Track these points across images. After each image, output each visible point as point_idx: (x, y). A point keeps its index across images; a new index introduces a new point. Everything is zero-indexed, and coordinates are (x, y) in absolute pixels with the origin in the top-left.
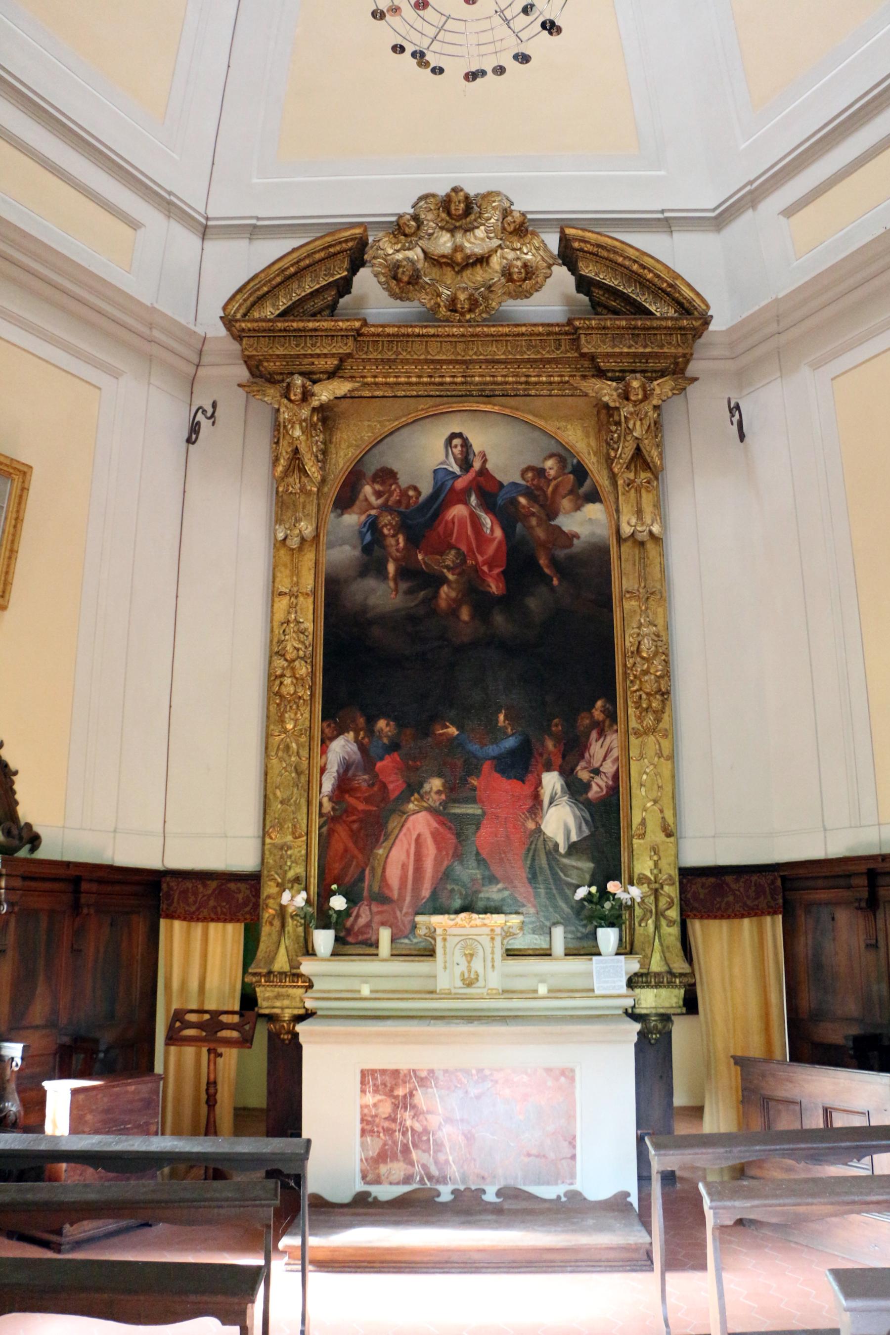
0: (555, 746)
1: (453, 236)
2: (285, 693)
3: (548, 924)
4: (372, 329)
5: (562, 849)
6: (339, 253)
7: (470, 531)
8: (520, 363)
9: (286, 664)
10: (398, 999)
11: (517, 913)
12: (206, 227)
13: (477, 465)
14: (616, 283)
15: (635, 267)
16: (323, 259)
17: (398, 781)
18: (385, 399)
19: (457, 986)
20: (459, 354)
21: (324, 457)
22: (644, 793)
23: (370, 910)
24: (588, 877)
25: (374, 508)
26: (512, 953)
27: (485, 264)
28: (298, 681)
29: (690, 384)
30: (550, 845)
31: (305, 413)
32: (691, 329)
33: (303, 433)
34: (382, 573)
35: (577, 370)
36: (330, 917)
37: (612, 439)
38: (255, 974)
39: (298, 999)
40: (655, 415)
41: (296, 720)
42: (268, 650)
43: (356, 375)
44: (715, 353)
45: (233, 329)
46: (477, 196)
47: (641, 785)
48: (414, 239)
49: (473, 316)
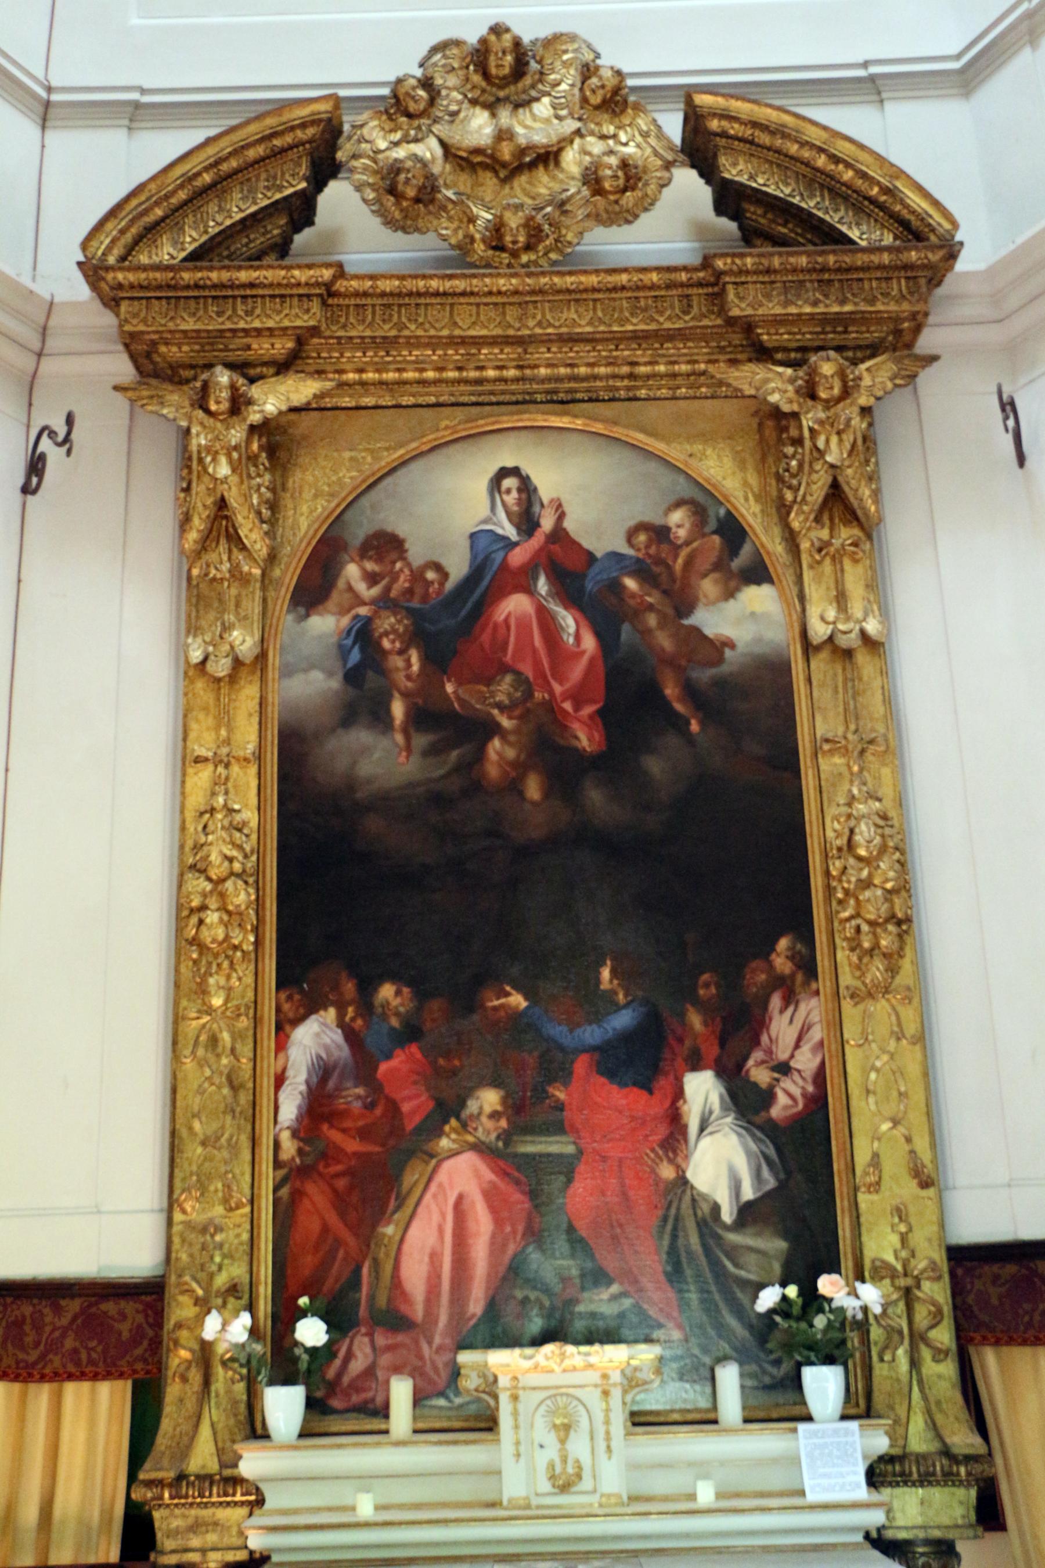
0: (705, 1024)
1: (493, 115)
2: (209, 940)
3: (707, 1360)
4: (354, 283)
5: (727, 1215)
6: (291, 147)
7: (538, 641)
8: (618, 340)
9: (209, 887)
10: (430, 1522)
11: (648, 1340)
12: (48, 104)
13: (547, 523)
14: (787, 191)
15: (821, 161)
16: (263, 159)
17: (417, 1096)
18: (379, 411)
19: (540, 1490)
20: (510, 326)
21: (273, 513)
22: (873, 1107)
23: (372, 1342)
24: (777, 1268)
25: (364, 604)
26: (642, 1419)
27: (552, 166)
28: (232, 916)
29: (923, 367)
30: (705, 1208)
31: (236, 435)
32: (924, 267)
33: (234, 470)
34: (381, 719)
35: (722, 349)
36: (296, 1360)
37: (787, 470)
38: (150, 1484)
39: (234, 1531)
40: (864, 425)
41: (229, 990)
42: (176, 860)
43: (329, 368)
44: (966, 311)
45: (103, 285)
46: (534, 43)
47: (868, 1092)
48: (425, 121)
49: (533, 257)
